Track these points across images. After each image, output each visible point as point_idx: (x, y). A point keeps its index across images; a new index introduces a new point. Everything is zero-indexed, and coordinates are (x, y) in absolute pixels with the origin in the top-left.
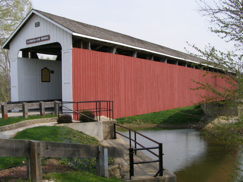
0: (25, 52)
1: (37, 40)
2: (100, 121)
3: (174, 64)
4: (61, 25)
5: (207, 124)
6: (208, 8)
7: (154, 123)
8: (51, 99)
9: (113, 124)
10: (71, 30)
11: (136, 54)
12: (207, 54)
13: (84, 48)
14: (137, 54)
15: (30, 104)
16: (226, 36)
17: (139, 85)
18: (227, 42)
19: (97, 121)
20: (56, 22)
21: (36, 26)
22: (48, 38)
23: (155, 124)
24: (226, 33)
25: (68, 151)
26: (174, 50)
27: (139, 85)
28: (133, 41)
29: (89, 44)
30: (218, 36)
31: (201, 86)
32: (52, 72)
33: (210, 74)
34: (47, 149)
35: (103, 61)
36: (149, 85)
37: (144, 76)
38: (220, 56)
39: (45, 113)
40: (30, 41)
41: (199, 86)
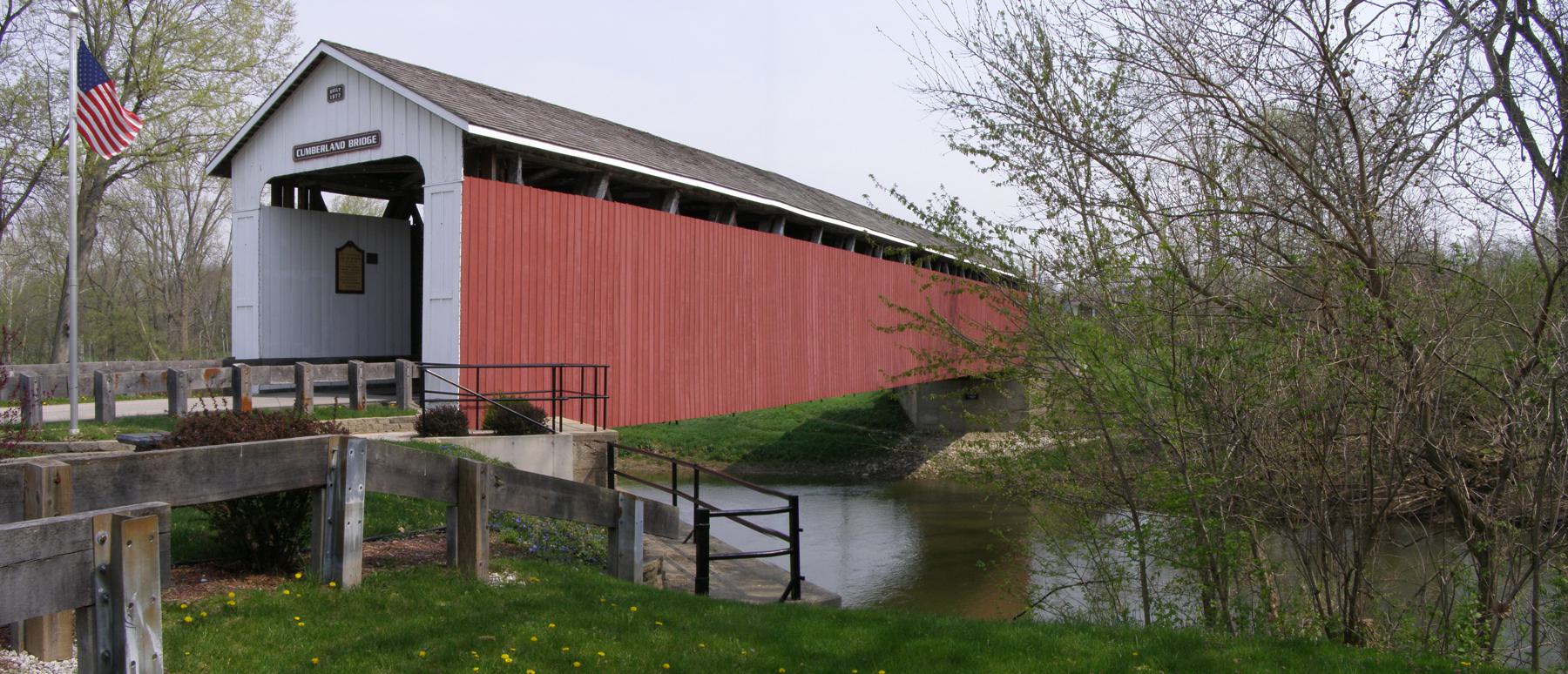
0: (281, 187)
1: (332, 147)
2: (561, 430)
3: (809, 240)
4: (425, 97)
5: (922, 460)
6: (945, 87)
7: (718, 459)
8: (388, 353)
9: (605, 446)
10: (463, 117)
11: (673, 204)
12: (937, 220)
13: (499, 179)
14: (680, 199)
15: (318, 367)
16: (995, 166)
17: (682, 313)
18: (999, 185)
19: (554, 433)
20: (405, 86)
21: (330, 100)
22: (373, 140)
23: (720, 464)
24: (995, 157)
25: (546, 498)
26: (809, 189)
27: (682, 313)
28: (665, 155)
29: (517, 164)
30: (972, 162)
31: (910, 319)
32: (373, 259)
33: (940, 283)
34: (497, 485)
35: (563, 225)
36: (719, 315)
37: (702, 280)
38: (973, 225)
39: (368, 400)
40: (308, 151)
41: (904, 319)
